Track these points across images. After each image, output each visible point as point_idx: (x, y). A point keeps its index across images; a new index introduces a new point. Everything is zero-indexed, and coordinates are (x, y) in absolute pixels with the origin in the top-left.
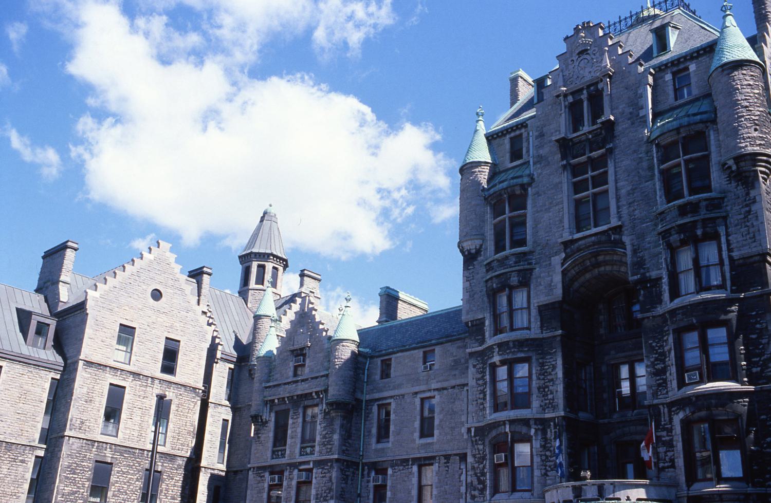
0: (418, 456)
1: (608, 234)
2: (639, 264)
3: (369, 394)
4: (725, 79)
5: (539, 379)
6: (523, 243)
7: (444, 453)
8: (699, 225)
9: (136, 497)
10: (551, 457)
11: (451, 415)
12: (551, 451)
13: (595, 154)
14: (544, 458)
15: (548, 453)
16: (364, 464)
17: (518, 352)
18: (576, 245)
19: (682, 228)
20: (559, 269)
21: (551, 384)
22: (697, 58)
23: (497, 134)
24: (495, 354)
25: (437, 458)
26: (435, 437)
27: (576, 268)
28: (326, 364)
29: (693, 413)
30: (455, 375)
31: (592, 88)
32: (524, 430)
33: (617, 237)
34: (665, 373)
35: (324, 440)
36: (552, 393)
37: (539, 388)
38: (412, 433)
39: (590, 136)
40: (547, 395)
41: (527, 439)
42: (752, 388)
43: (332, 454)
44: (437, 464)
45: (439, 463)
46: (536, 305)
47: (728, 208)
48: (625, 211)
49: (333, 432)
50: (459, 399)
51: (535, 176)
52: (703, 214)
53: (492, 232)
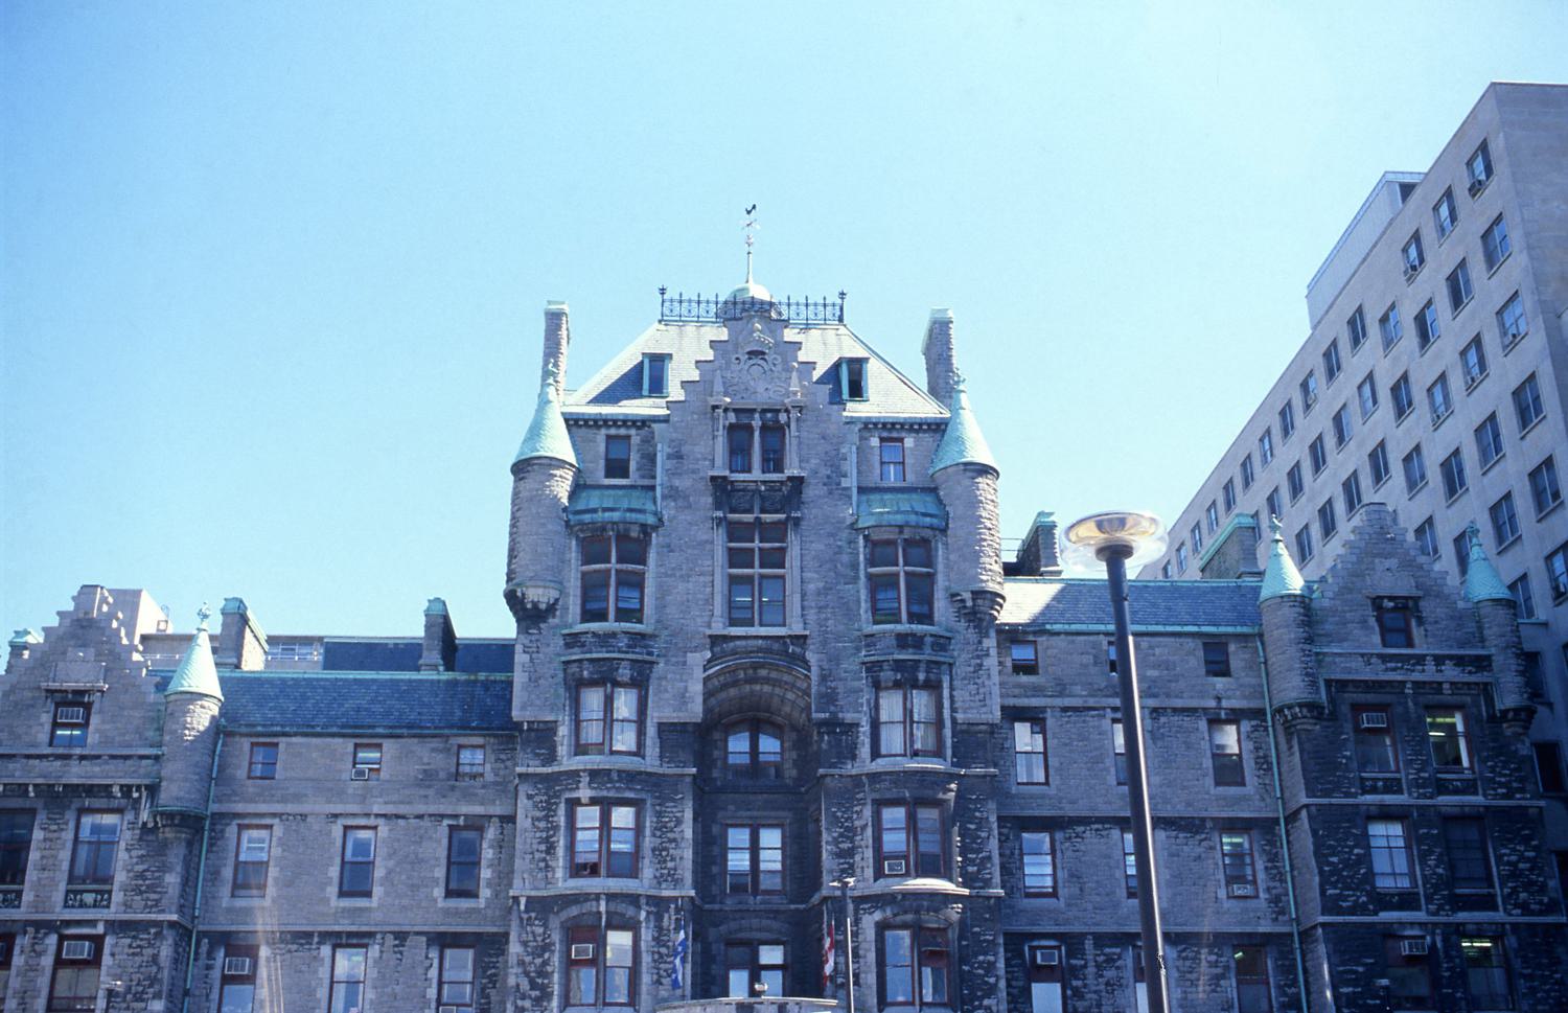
0: (337, 928)
1: (785, 643)
2: (829, 698)
3: (220, 801)
4: (967, 482)
5: (654, 835)
6: (635, 614)
7: (397, 929)
8: (923, 666)
9: (1060, 1010)
10: (668, 956)
11: (412, 863)
12: (668, 947)
13: (768, 517)
14: (656, 956)
15: (663, 950)
16: (202, 934)
17: (625, 789)
18: (732, 645)
19: (899, 665)
20: (699, 674)
21: (673, 845)
22: (917, 431)
23: (586, 421)
24: (581, 785)
25: (379, 936)
26: (375, 898)
27: (722, 678)
28: (150, 734)
29: (895, 915)
30: (426, 796)
31: (769, 415)
32: (630, 912)
33: (798, 650)
34: (852, 857)
35: (140, 882)
36: (673, 859)
37: (654, 850)
38: (323, 887)
39: (763, 488)
40: (665, 861)
41: (631, 925)
42: (966, 892)
43: (163, 911)
44: (377, 947)
45: (382, 945)
46: (655, 720)
47: (956, 654)
48: (812, 616)
49: (164, 868)
50: (431, 838)
51: (665, 518)
52: (927, 655)
53: (579, 583)
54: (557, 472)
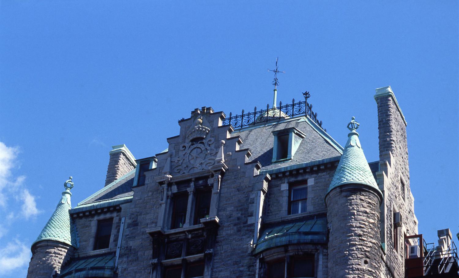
4: (342, 201)
22: (317, 172)
39: (190, 236)
54: (53, 250)
